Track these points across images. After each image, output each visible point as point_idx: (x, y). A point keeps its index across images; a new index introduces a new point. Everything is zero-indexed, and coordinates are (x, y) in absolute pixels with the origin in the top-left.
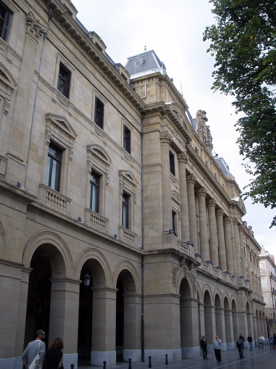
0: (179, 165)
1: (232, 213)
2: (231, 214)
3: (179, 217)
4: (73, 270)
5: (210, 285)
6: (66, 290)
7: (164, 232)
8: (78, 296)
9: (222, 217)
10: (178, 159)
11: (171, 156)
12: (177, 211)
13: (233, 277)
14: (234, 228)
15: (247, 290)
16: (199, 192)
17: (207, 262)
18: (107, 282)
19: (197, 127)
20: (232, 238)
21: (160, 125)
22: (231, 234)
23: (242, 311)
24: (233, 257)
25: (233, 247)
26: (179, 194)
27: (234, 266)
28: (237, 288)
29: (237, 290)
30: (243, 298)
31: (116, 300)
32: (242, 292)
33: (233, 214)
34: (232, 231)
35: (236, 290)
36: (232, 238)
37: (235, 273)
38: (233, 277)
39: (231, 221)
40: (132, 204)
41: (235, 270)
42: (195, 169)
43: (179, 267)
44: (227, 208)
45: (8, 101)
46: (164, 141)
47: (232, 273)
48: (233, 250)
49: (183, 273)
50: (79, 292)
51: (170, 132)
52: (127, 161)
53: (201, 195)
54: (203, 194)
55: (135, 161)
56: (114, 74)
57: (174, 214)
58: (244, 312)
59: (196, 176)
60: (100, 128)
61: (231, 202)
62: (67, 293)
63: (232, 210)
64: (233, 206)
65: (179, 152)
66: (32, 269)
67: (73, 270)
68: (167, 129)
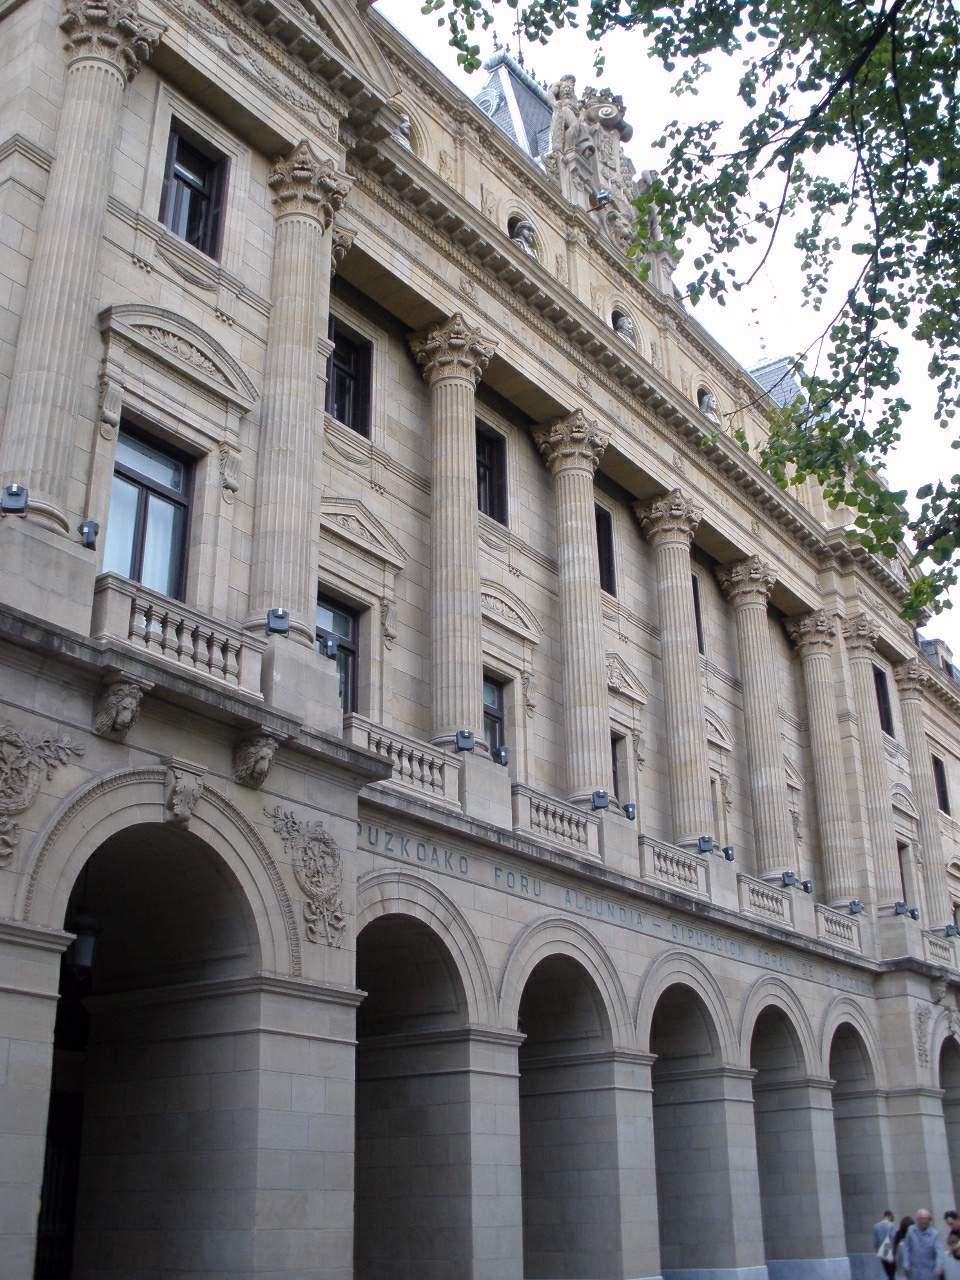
0: (901, 700)
1: (834, 593)
2: (831, 599)
3: (915, 856)
4: (492, 1005)
5: (797, 985)
6: (262, 1027)
7: (880, 909)
8: (48, 1015)
9: (762, 600)
10: (897, 681)
11: (879, 676)
12: (908, 841)
13: (853, 913)
14: (853, 666)
15: (938, 974)
16: (653, 516)
17: (780, 883)
18: (471, 1009)
19: (551, 146)
20: (843, 717)
21: (841, 596)
22: (837, 697)
23: (908, 1083)
24: (855, 808)
25: (848, 759)
26: (910, 789)
27: (861, 854)
28: (874, 967)
29: (877, 977)
30: (913, 1022)
31: (55, 1004)
32: (905, 988)
33: (847, 599)
34: (842, 682)
35: (867, 978)
36: (843, 717)
37: (864, 887)
38: (853, 909)
39: (832, 635)
40: (519, 712)
41: (863, 873)
42: (767, 537)
43: (931, 1006)
44: (809, 574)
45: (232, 453)
46: (855, 644)
47: (846, 893)
48: (850, 774)
49: (945, 1024)
50: (56, 994)
51: (870, 616)
52: (494, 553)
53: (745, 593)
54: (754, 587)
55: (387, 462)
56: (600, 339)
57: (902, 847)
58: (917, 1092)
59: (698, 501)
60: (362, 438)
61: (826, 539)
62: (264, 1039)
63: (835, 581)
64: (844, 561)
65: (896, 659)
66: (366, 994)
67: (492, 1005)
68: (862, 609)
